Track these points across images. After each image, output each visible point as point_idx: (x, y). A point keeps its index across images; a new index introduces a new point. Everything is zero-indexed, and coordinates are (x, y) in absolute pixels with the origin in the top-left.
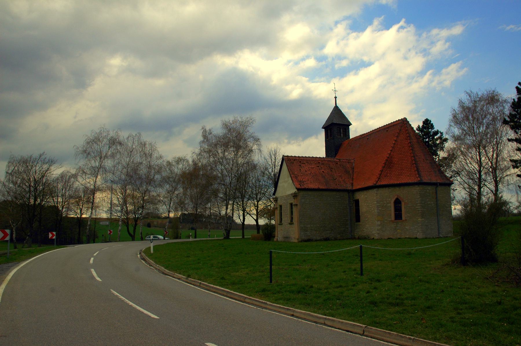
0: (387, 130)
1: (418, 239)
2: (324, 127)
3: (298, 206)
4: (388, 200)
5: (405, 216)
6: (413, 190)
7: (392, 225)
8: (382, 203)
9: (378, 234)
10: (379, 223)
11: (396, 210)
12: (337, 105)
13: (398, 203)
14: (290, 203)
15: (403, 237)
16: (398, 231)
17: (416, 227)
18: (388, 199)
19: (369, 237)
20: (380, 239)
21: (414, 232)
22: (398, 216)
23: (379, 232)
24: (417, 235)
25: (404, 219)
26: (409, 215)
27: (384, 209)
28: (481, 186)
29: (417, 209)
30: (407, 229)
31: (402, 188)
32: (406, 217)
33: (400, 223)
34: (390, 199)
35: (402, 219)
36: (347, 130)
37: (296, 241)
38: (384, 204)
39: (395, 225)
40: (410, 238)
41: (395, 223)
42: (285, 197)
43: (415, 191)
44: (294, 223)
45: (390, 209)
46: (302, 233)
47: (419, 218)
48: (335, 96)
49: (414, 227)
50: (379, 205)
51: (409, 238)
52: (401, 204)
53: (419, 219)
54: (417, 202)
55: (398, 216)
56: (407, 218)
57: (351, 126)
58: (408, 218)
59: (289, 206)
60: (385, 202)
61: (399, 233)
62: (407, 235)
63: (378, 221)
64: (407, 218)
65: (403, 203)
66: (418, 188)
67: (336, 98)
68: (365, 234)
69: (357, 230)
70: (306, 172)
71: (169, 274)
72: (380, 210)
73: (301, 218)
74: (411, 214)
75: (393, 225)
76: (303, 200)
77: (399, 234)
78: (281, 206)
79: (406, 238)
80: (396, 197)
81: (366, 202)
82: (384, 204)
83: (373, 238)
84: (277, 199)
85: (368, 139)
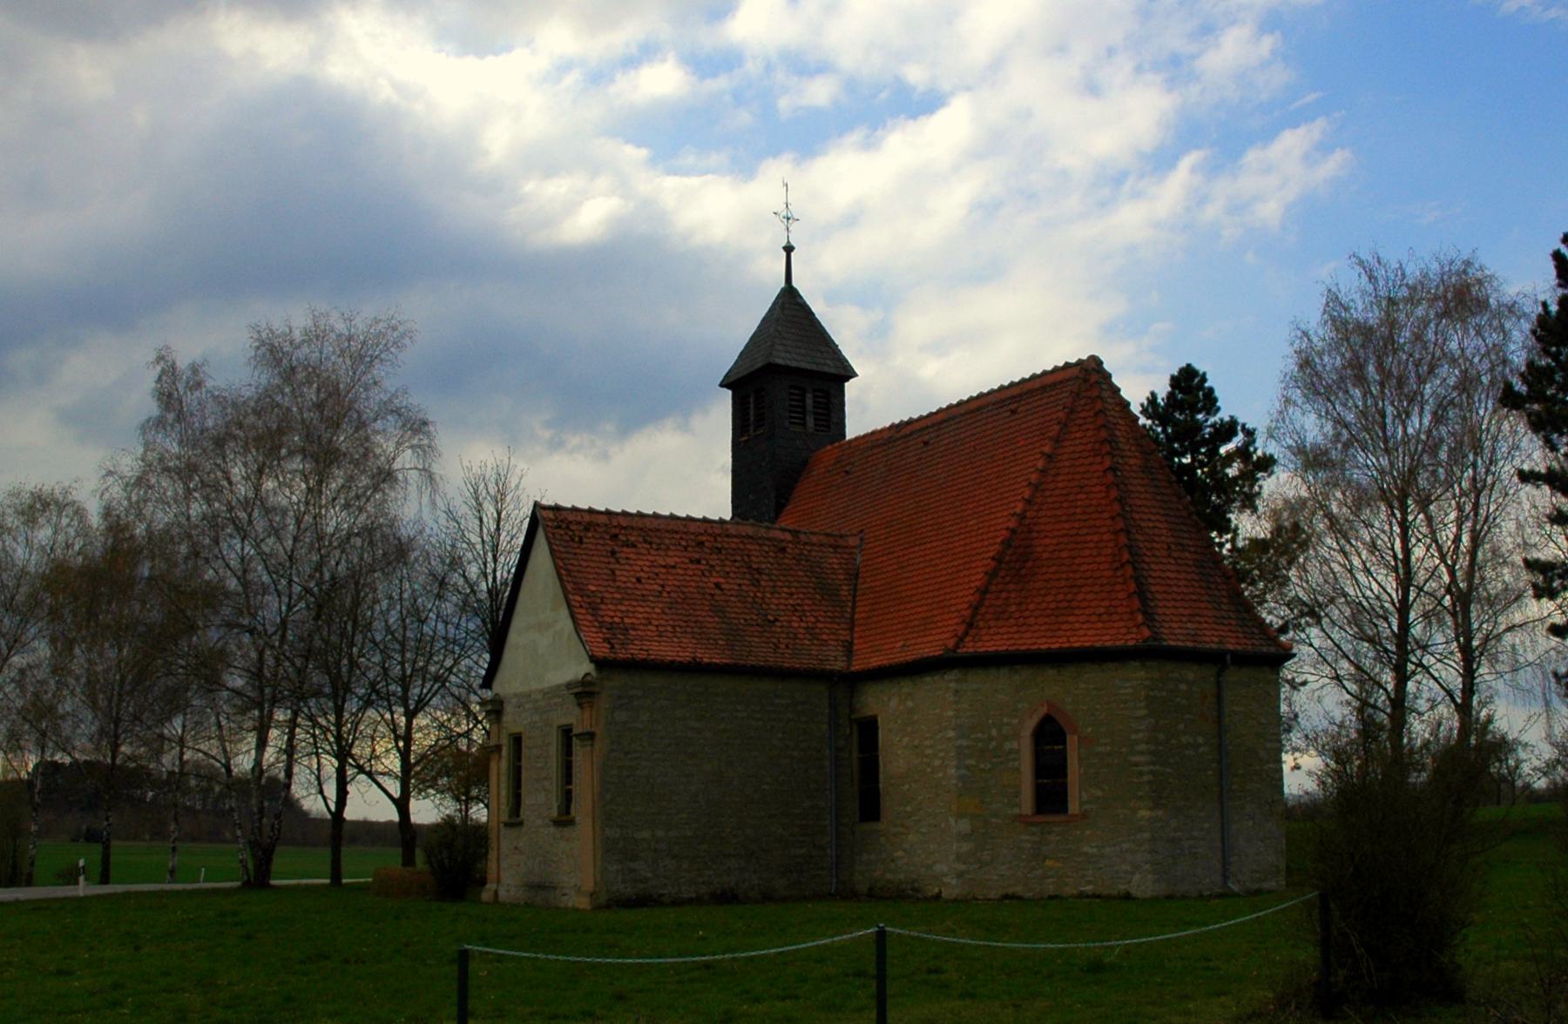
4: (1007, 724)
5: (1080, 797)
7: (1023, 837)
8: (979, 735)
9: (960, 875)
10: (965, 826)
11: (1061, 770)
13: (1050, 735)
14: (559, 727)
15: (1070, 890)
17: (1126, 846)
23: (963, 867)
26: (1099, 793)
27: (989, 766)
29: (1136, 764)
30: (1086, 854)
38: (991, 739)
40: (1099, 896)
41: (1034, 829)
42: (540, 697)
43: (1128, 685)
44: (578, 819)
45: (1016, 763)
48: (784, 244)
50: (965, 743)
52: (1064, 742)
53: (1144, 813)
57: (852, 380)
60: (994, 732)
61: (1050, 873)
62: (1089, 882)
63: (960, 816)
64: (1087, 807)
67: (789, 249)
72: (967, 767)
75: (1027, 837)
76: (622, 716)
78: (517, 740)
79: (1081, 895)
80: (1044, 710)
82: (991, 739)
83: (938, 896)
85: (926, 443)
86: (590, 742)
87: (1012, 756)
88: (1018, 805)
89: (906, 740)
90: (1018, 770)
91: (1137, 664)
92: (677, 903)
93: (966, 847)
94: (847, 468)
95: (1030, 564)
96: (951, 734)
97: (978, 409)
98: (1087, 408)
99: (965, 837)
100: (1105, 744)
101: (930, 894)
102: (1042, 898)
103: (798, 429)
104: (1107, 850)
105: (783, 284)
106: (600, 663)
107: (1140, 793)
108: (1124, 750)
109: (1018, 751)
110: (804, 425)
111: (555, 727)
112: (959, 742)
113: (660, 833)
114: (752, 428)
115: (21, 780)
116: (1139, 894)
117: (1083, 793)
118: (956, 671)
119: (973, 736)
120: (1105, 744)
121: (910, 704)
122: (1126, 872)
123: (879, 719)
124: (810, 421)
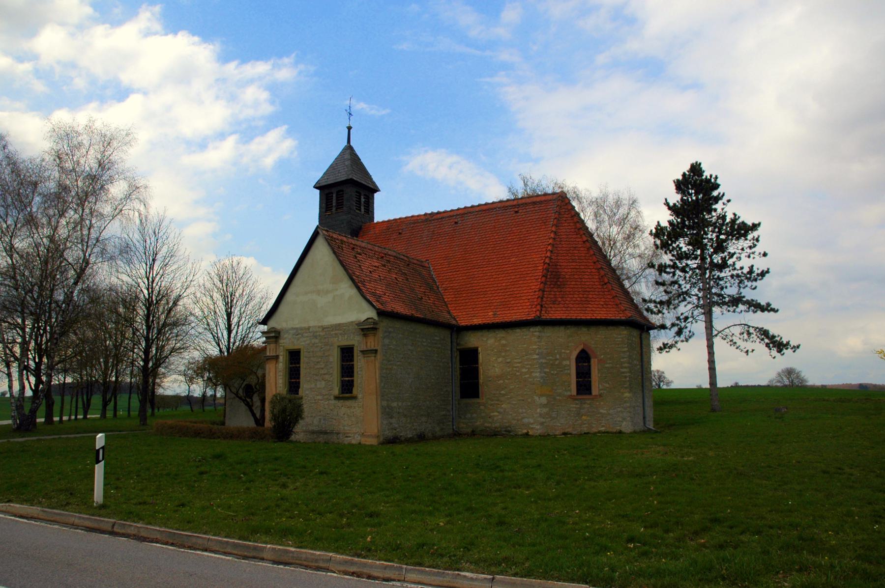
0: (516, 210)
1: (625, 433)
2: (321, 185)
3: (379, 356)
4: (564, 353)
6: (615, 336)
7: (572, 406)
8: (551, 358)
9: (542, 424)
10: (544, 400)
11: (579, 375)
12: (351, 144)
13: (584, 358)
14: (338, 346)
15: (594, 430)
16: (583, 417)
17: (619, 409)
18: (563, 351)
19: (509, 432)
20: (546, 434)
21: (616, 421)
22: (584, 386)
24: (621, 426)
25: (597, 394)
27: (556, 372)
28: (712, 333)
29: (623, 373)
30: (601, 413)
31: (593, 329)
32: (602, 389)
33: (588, 402)
34: (568, 351)
35: (590, 393)
36: (371, 201)
37: (373, 442)
38: (556, 359)
39: (578, 406)
40: (607, 432)
41: (577, 402)
42: (320, 330)
43: (619, 337)
44: (360, 396)
45: (569, 372)
46: (385, 422)
47: (625, 393)
48: (348, 126)
49: (615, 410)
50: (544, 361)
51: (604, 432)
52: (589, 362)
53: (627, 395)
54: (622, 360)
55: (584, 386)
56: (602, 392)
57: (378, 193)
58: (605, 392)
59: (335, 357)
60: (558, 356)
61: (585, 422)
62: (603, 426)
63: (541, 395)
64: (602, 392)
65: (594, 362)
66: (625, 332)
67: (349, 128)
68: (498, 425)
69: (469, 416)
70: (371, 275)
71: (153, 536)
72: (545, 373)
73: (382, 385)
74: (610, 383)
75: (574, 406)
76: (387, 341)
77: (585, 424)
78: (294, 356)
79: (599, 432)
80: (581, 347)
81: (503, 354)
82: (556, 359)
83: (527, 434)
84: (278, 335)
85: (456, 223)
86: (374, 355)
87: (566, 368)
88: (570, 390)
89: (500, 360)
90: (569, 374)
91: (623, 328)
92: (436, 438)
93: (545, 410)
94: (400, 231)
95: (561, 280)
96: (536, 357)
97: (541, 202)
98: (566, 213)
99: (544, 406)
100: (610, 363)
101: (520, 433)
102: (581, 434)
103: (358, 212)
104: (611, 411)
105: (346, 144)
106: (380, 313)
107: (625, 386)
108: (618, 366)
109: (569, 366)
110: (360, 210)
111: (336, 347)
112: (541, 360)
113: (400, 404)
114: (334, 209)
115: (786, 386)
116: (626, 431)
117: (600, 385)
118: (539, 327)
119: (547, 358)
120: (610, 363)
121: (504, 342)
122: (619, 421)
123: (479, 349)
124: (363, 210)
